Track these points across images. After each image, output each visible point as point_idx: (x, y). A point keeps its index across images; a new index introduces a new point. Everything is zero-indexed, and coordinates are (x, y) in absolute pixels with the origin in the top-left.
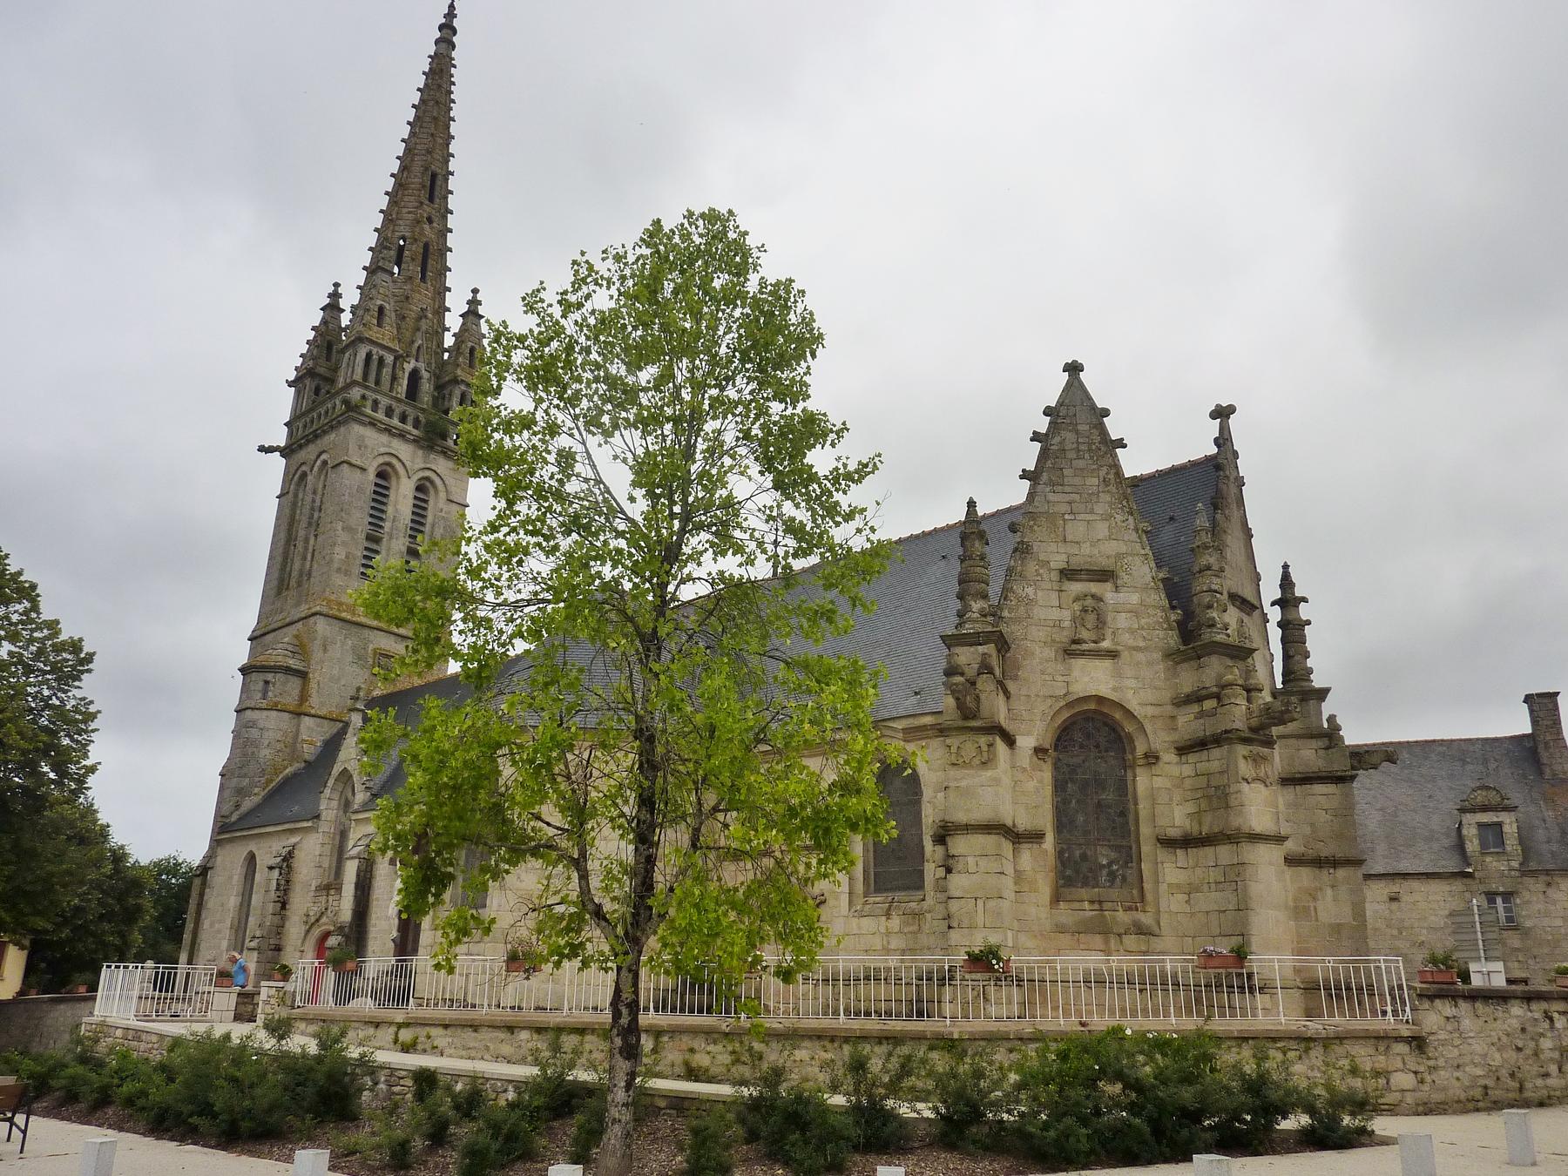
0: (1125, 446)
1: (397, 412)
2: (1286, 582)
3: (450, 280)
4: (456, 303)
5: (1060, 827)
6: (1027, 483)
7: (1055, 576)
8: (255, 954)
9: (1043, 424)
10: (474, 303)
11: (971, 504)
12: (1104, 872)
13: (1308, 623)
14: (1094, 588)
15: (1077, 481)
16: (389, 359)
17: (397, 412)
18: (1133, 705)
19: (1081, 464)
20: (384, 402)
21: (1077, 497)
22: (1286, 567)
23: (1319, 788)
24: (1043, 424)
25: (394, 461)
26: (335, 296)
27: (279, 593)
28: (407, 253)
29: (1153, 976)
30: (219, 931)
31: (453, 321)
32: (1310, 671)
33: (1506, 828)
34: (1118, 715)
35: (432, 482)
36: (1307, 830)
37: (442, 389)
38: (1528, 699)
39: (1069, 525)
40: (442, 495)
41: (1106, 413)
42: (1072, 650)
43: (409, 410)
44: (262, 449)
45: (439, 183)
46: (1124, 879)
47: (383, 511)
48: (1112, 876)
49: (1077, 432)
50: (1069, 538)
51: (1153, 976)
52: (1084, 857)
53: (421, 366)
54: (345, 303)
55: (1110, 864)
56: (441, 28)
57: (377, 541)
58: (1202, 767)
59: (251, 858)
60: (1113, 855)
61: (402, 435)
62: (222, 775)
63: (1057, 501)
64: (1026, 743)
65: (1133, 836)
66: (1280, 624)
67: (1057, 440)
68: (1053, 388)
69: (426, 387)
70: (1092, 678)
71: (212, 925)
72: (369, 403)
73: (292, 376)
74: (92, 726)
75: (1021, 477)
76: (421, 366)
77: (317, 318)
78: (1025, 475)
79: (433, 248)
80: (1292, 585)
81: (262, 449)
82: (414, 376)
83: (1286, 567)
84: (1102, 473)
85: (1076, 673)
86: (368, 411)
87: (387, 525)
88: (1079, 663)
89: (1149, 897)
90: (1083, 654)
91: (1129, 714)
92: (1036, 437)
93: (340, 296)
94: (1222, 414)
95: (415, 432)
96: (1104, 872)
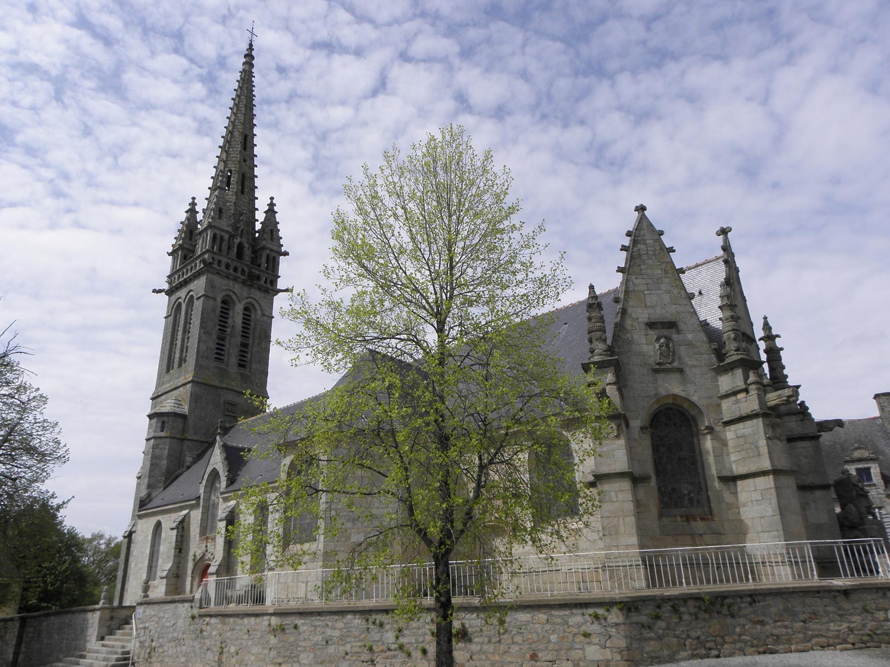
0: (674, 251)
1: (232, 266)
2: (767, 326)
3: (257, 194)
4: (261, 205)
5: (658, 473)
6: (621, 274)
7: (643, 326)
8: (165, 580)
9: (627, 241)
10: (272, 205)
11: (591, 287)
12: (687, 498)
13: (782, 349)
14: (666, 332)
15: (649, 271)
16: (226, 237)
17: (232, 266)
18: (695, 399)
19: (650, 262)
20: (224, 260)
21: (650, 281)
22: (765, 318)
24: (627, 241)
25: (231, 294)
26: (193, 204)
27: (168, 371)
28: (232, 179)
30: (141, 569)
31: (260, 216)
32: (786, 376)
33: (872, 471)
34: (686, 406)
35: (253, 305)
37: (255, 252)
38: (877, 397)
39: (648, 296)
40: (259, 312)
41: (661, 233)
42: (658, 370)
43: (238, 264)
44: (154, 291)
45: (248, 140)
46: (698, 501)
47: (226, 322)
48: (691, 499)
49: (646, 244)
50: (649, 304)
52: (674, 490)
53: (244, 240)
54: (199, 208)
55: (689, 493)
56: (246, 56)
57: (223, 339)
58: (740, 432)
59: (158, 525)
61: (235, 279)
62: (139, 478)
63: (639, 283)
66: (765, 351)
68: (630, 221)
69: (247, 252)
70: (672, 386)
71: (136, 565)
72: (216, 262)
73: (170, 250)
74: (509, 201)
75: (618, 271)
76: (244, 240)
77: (183, 216)
78: (620, 270)
79: (247, 176)
80: (770, 329)
81: (154, 291)
82: (240, 247)
83: (765, 318)
84: (663, 266)
86: (216, 266)
87: (229, 330)
88: (661, 376)
89: (715, 511)
91: (693, 404)
92: (624, 248)
93: (196, 204)
94: (724, 232)
95: (242, 277)
96: (687, 498)
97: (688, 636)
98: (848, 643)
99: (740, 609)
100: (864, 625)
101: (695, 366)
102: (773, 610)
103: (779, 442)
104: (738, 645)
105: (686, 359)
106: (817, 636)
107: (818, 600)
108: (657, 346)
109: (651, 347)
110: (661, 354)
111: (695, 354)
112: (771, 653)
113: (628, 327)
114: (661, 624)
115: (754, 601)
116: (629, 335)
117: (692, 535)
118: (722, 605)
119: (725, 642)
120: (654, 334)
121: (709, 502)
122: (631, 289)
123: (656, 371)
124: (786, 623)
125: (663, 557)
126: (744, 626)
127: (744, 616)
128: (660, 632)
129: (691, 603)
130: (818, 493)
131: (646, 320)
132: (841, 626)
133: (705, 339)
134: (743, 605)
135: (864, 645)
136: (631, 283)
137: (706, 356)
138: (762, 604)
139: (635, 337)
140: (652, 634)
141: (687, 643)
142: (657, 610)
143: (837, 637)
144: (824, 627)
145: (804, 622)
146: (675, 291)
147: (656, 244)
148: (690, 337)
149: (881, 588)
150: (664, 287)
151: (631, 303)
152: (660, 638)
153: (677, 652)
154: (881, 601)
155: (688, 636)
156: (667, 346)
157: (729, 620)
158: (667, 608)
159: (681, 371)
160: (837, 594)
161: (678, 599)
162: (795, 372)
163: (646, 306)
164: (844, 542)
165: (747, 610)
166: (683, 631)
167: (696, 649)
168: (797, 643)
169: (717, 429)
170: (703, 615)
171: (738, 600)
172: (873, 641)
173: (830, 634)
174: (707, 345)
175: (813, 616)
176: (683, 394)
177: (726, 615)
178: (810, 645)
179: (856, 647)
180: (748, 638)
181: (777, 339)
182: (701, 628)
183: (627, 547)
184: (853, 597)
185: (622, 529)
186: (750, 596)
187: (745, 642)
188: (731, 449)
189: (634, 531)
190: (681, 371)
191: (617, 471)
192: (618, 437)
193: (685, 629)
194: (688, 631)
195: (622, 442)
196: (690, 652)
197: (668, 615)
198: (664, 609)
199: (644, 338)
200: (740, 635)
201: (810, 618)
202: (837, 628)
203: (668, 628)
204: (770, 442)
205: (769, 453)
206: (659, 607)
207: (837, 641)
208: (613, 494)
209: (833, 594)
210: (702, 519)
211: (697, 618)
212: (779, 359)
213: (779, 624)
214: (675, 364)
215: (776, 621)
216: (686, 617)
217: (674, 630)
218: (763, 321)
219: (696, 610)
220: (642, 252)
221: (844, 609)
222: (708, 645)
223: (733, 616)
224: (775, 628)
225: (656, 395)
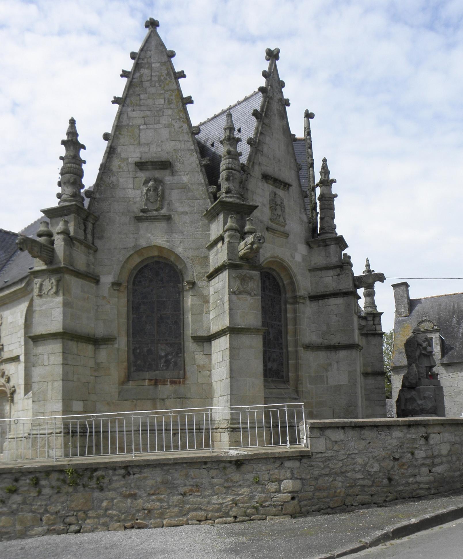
0: (184, 76)
7: (132, 167)
12: (163, 360)
14: (158, 174)
15: (150, 102)
18: (180, 250)
19: (153, 90)
21: (148, 113)
22: (72, 122)
23: (333, 301)
29: (160, 425)
34: (172, 259)
36: (325, 328)
41: (172, 55)
42: (143, 217)
46: (176, 364)
48: (167, 362)
50: (143, 141)
51: (160, 425)
55: (166, 356)
60: (169, 349)
63: (135, 116)
64: (107, 280)
65: (182, 336)
67: (137, 75)
70: (155, 236)
78: (116, 101)
83: (72, 122)
85: (142, 232)
88: (144, 226)
90: (147, 219)
91: (177, 256)
92: (125, 74)
96: (163, 360)
97: (46, 511)
98: (230, 517)
99: (110, 482)
100: (251, 498)
101: (187, 213)
102: (150, 482)
103: (249, 298)
104: (102, 520)
105: (177, 205)
106: (195, 510)
107: (205, 472)
108: (145, 190)
109: (138, 192)
110: (147, 199)
111: (188, 199)
112: (139, 528)
113: (115, 169)
114: (17, 498)
115: (129, 474)
116: (114, 179)
117: (154, 400)
118: (91, 478)
119: (87, 517)
120: (142, 175)
121: (184, 365)
122: (124, 123)
123: (139, 219)
124: (163, 496)
125: (113, 422)
126: (113, 499)
127: (115, 490)
128: (15, 506)
129: (54, 476)
130: (343, 353)
131: (137, 160)
132: (225, 498)
133: (203, 181)
134: (115, 478)
135: (247, 518)
136: (125, 117)
137: (201, 201)
138: (137, 476)
139: (121, 180)
140: (5, 509)
141: (44, 518)
142: (15, 483)
143: (218, 510)
144: (205, 500)
145: (184, 495)
146: (177, 125)
147: (164, 68)
148: (185, 179)
149: (279, 458)
150: (164, 120)
151: (122, 140)
152: (13, 513)
153: (32, 527)
154: (276, 471)
155: (46, 511)
156: (155, 189)
157: (96, 494)
158: (25, 482)
159: (168, 218)
160: (228, 465)
161: (40, 472)
162: (345, 222)
163: (139, 144)
164: (252, 408)
165: (118, 482)
166: (41, 506)
167: (53, 524)
168: (171, 517)
169: (200, 284)
170: (66, 489)
171: (111, 472)
172: (257, 514)
173: (211, 507)
174: (204, 189)
175: (194, 489)
176: (166, 245)
177: (93, 488)
178: (185, 519)
179: (238, 520)
180: (114, 512)
181: (82, 150)
182: (62, 503)
183: (52, 413)
184: (244, 468)
185: (49, 395)
186: (126, 467)
187: (111, 517)
188: (211, 306)
189: (60, 397)
190: (168, 218)
191: (52, 332)
192: (56, 293)
193: (44, 503)
194: (46, 505)
195: (60, 299)
196: (46, 528)
197: (25, 489)
198: (21, 483)
199: (131, 181)
200: (106, 510)
201: (191, 491)
202: (220, 501)
203: (24, 503)
204: (234, 297)
205: (230, 309)
206: (16, 480)
207: (217, 514)
208: (46, 357)
209: (222, 465)
210: (173, 382)
211: (58, 492)
212: (332, 208)
213: (154, 497)
214: (164, 211)
215: (150, 495)
216: (47, 491)
217: (31, 505)
218: (68, 125)
219: (59, 483)
220: (145, 78)
221: (232, 481)
222: (68, 520)
223: (101, 489)
224: (148, 502)
225: (134, 247)
